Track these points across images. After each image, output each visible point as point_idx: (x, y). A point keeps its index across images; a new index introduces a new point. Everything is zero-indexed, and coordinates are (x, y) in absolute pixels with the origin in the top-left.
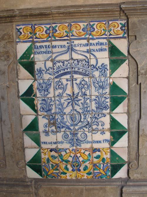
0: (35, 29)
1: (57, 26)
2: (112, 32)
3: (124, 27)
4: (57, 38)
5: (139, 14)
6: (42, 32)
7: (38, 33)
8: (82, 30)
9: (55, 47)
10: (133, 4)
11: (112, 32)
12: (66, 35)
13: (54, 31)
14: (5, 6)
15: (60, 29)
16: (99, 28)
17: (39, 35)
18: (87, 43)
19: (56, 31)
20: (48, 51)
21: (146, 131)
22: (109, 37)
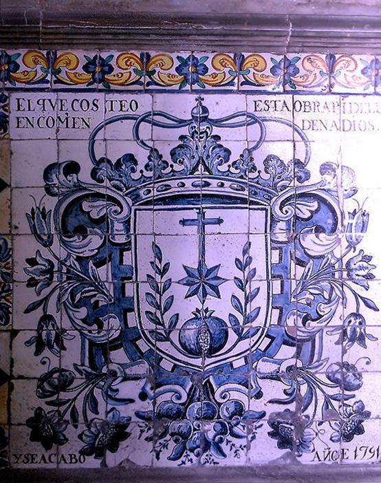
0: (244, 60)
1: (20, 54)
2: (62, 76)
3: (93, 65)
4: (208, 87)
5: (121, 42)
6: (73, 69)
7: (64, 70)
8: (177, 69)
9: (91, 105)
10: (144, 20)
11: (62, 76)
12: (134, 80)
13: (291, 70)
14: (7, 8)
15: (122, 63)
16: (219, 66)
17: (255, 78)
18: (209, 100)
19: (111, 69)
20: (344, 120)
21: (219, 482)
22: (146, 88)
